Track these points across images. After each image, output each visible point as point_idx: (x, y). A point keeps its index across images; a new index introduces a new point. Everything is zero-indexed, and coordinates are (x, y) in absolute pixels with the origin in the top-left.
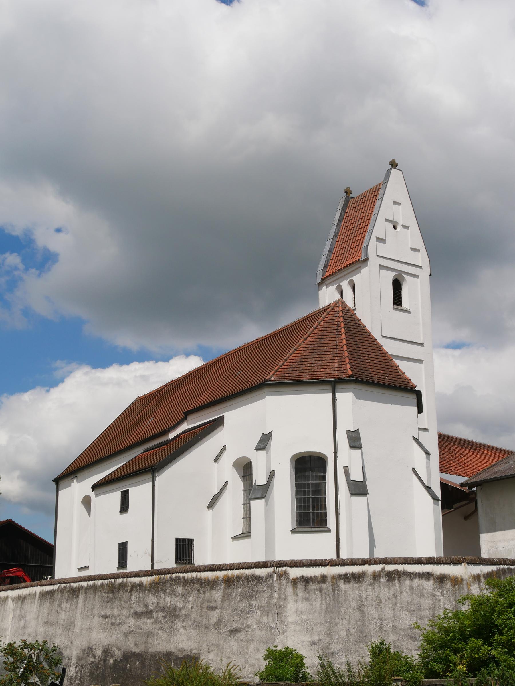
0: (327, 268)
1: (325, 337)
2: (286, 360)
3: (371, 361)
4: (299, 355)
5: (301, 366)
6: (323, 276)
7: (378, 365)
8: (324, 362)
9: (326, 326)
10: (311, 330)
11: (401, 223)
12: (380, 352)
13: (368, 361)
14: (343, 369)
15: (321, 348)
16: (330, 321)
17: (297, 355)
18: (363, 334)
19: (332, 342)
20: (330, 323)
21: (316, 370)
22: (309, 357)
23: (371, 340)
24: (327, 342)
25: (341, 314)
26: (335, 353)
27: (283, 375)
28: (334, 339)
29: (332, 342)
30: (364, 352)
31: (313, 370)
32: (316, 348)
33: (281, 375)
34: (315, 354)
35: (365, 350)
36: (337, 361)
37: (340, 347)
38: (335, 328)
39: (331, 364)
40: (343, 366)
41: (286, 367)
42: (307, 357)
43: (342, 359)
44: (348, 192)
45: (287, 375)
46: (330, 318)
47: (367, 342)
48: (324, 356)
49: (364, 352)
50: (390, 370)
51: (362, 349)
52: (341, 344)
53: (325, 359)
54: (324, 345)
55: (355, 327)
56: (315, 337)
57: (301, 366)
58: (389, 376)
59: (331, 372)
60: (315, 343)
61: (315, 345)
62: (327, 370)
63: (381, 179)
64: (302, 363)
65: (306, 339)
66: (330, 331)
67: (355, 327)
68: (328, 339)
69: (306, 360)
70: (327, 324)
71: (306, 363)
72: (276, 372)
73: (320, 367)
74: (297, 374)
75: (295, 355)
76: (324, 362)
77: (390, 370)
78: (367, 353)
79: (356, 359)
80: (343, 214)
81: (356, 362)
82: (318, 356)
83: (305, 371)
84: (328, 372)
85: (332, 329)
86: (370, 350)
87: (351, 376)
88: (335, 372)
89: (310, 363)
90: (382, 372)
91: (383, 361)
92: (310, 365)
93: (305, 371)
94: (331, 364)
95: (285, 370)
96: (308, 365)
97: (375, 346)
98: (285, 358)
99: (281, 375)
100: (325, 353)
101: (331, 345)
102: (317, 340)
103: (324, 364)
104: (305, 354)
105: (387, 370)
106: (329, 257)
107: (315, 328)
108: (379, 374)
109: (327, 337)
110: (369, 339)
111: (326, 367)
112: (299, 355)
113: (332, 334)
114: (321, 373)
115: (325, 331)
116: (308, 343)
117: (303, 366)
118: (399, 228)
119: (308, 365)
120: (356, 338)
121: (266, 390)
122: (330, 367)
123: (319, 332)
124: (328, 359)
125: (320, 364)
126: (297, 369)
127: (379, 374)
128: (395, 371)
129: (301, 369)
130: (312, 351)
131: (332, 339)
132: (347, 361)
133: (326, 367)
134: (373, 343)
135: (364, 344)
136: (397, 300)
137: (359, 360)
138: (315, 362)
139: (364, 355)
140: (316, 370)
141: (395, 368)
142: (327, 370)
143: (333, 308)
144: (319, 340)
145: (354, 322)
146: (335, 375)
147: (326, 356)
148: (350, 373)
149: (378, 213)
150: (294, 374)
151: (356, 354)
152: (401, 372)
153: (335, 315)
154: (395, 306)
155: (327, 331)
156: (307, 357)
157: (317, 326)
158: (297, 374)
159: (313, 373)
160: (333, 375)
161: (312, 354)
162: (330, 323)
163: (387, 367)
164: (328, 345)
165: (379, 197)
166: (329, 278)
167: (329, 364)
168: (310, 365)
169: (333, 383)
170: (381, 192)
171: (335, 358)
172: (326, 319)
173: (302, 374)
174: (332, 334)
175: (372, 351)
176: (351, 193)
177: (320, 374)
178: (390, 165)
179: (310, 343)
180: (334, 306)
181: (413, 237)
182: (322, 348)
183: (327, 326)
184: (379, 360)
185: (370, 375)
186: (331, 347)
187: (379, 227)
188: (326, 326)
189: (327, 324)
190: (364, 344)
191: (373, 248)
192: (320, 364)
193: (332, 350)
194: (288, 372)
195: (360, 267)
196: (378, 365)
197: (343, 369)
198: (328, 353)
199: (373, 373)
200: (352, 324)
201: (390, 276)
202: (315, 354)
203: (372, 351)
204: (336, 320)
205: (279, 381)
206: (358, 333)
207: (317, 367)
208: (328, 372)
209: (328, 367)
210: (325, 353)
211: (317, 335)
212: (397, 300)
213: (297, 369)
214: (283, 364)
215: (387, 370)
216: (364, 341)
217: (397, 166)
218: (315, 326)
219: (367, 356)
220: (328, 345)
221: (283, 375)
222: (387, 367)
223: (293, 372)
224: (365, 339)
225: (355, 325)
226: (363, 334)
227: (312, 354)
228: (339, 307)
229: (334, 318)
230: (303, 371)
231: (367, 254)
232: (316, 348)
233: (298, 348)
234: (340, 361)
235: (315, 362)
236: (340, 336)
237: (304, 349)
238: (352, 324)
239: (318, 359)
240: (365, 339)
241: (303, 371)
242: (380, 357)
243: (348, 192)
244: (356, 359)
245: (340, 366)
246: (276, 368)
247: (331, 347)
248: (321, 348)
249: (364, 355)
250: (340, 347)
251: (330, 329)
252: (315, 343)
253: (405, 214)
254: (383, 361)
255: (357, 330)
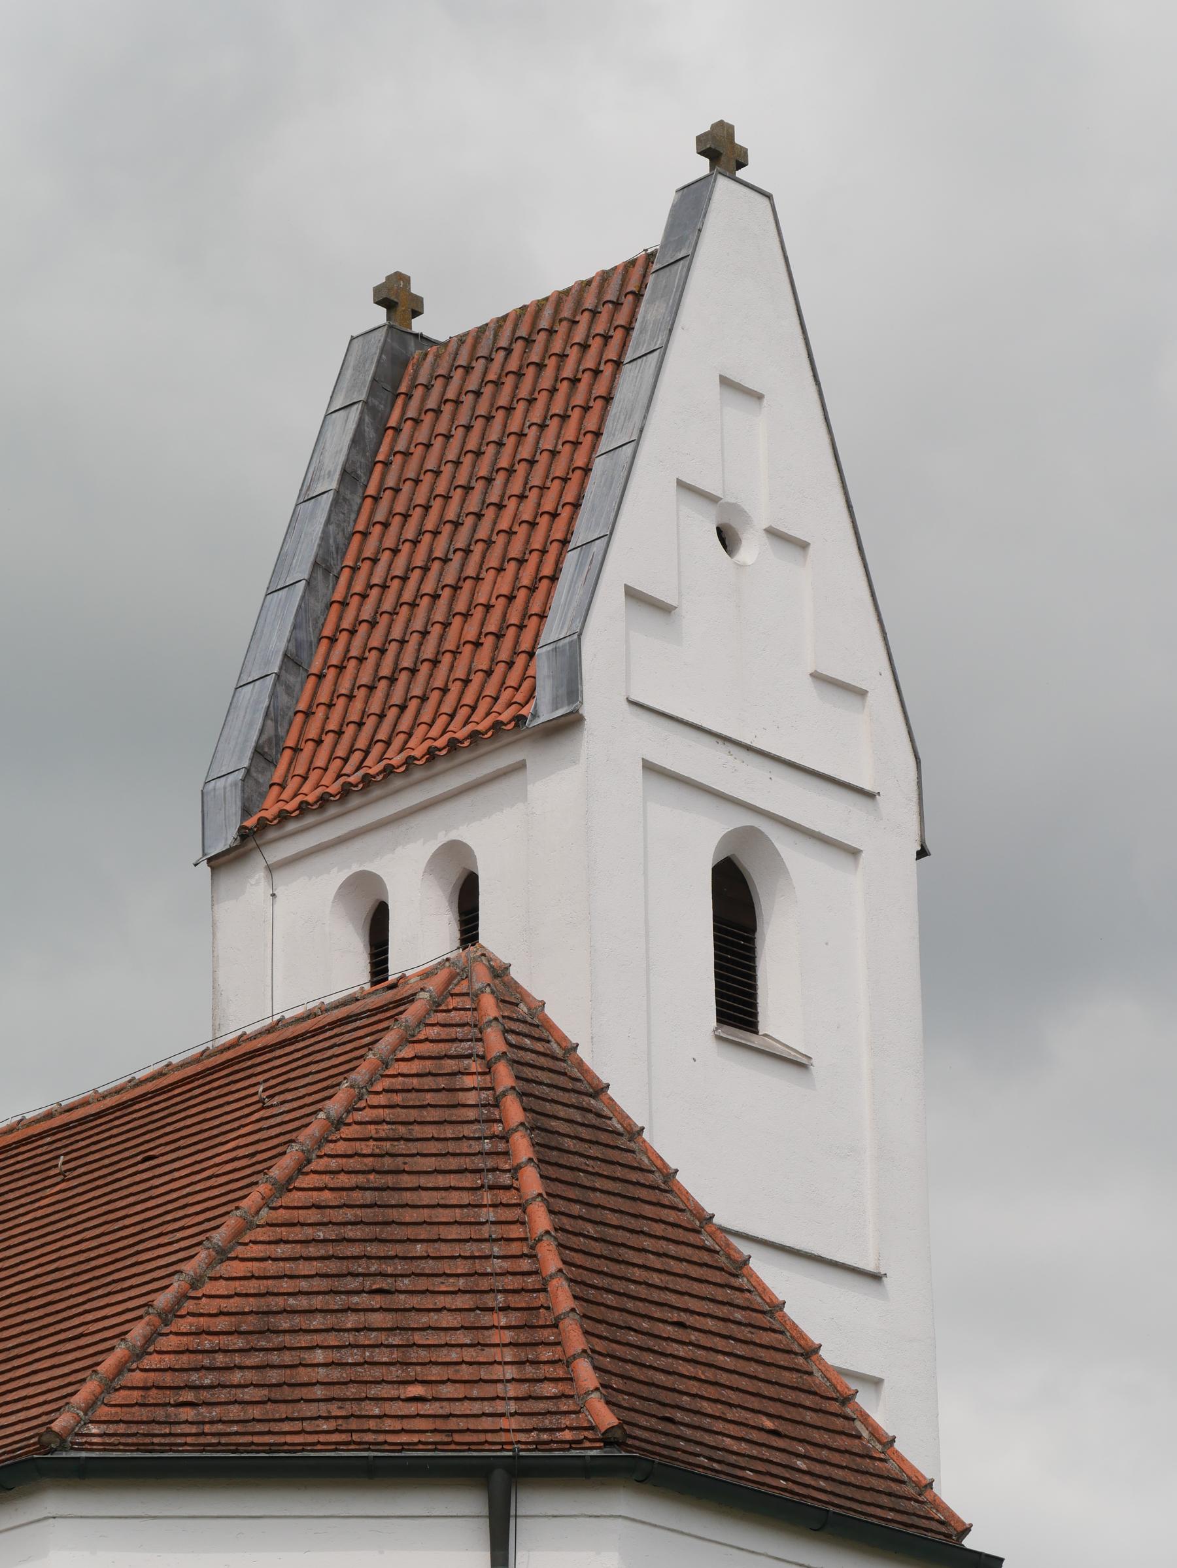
0: (273, 763)
1: (407, 1181)
2: (170, 1314)
3: (700, 1354)
4: (252, 1286)
5: (275, 1358)
6: (246, 812)
7: (744, 1383)
8: (418, 1338)
9: (403, 1115)
10: (315, 1128)
11: (761, 512)
12: (738, 1298)
13: (681, 1351)
14: (551, 1389)
15: (391, 1250)
16: (429, 1082)
17: (240, 1286)
18: (634, 1176)
19: (458, 1214)
20: (430, 1098)
21: (373, 1391)
22: (318, 1302)
23: (683, 1219)
24: (425, 1214)
25: (495, 1042)
26: (484, 1284)
27: (160, 1414)
28: (466, 1198)
29: (458, 1214)
30: (656, 1295)
31: (352, 1391)
32: (354, 1250)
33: (143, 1414)
34: (354, 1284)
35: (656, 1279)
36: (507, 1336)
37: (515, 1248)
38: (467, 1130)
39: (469, 1354)
40: (549, 1371)
41: (168, 1361)
42: (304, 1302)
43: (535, 1326)
44: (397, 298)
45: (188, 1413)
46: (429, 1065)
47: (658, 1229)
48: (414, 1301)
49: (656, 1295)
50: (809, 1417)
51: (638, 1274)
52: (516, 1231)
53: (424, 1319)
54: (411, 1232)
55: (584, 1133)
56: (343, 1180)
57: (275, 1358)
58: (813, 1452)
59: (476, 1407)
60: (349, 1214)
61: (350, 1232)
62: (447, 1391)
63: (647, 234)
64: (277, 1340)
65: (286, 1186)
66: (433, 1147)
67: (584, 1133)
68: (427, 1198)
69: (298, 1321)
70: (413, 1099)
71: (304, 1340)
72: (109, 1386)
73: (395, 1373)
74: (256, 1412)
75: (221, 1287)
76: (418, 1338)
77: (809, 1417)
78: (673, 1299)
79: (620, 1335)
80: (370, 433)
81: (619, 1350)
82: (376, 1301)
83: (305, 1393)
84: (458, 1408)
85: (449, 1132)
86: (683, 1285)
87: (608, 1440)
88: (500, 1407)
89: (332, 1339)
90: (769, 1424)
91: (763, 1354)
92: (335, 1356)
93: (305, 1393)
94: (469, 1354)
95: (168, 1379)
96: (319, 1356)
97: (706, 1257)
98: (162, 1300)
99: (143, 1414)
100: (422, 1284)
101: (454, 1232)
102: (357, 1197)
103: (423, 1355)
104: (286, 1285)
105: (794, 1413)
106: (284, 699)
107: (339, 1123)
108: (754, 1435)
109: (423, 1181)
110: (672, 1216)
111: (435, 1373)
112: (252, 1286)
113: (453, 1163)
114: (412, 1408)
115: (401, 1147)
116: (303, 1216)
117: (287, 1358)
118: (752, 548)
119: (319, 1356)
120: (597, 1198)
121: (51, 1503)
122: (465, 1372)
123: (367, 1148)
124: (447, 1320)
125: (396, 1355)
126: (249, 1376)
127: (754, 1435)
128: (839, 1423)
129: (274, 1376)
130: (332, 1267)
131: (454, 1198)
132: (575, 1340)
133: (435, 1373)
134: (691, 1238)
135: (647, 1243)
136: (737, 1003)
137: (632, 1338)
138: (362, 1339)
139: (656, 1312)
140: (373, 1391)
141: (834, 1407)
142: (447, 1391)
143: (436, 1006)
144: (369, 1197)
145: (573, 1099)
146: (509, 1428)
147: (427, 1302)
148: (607, 1418)
149: (637, 442)
150: (235, 1412)
151: (610, 1299)
152: (875, 1431)
153: (454, 1049)
154: (720, 1032)
155: (414, 1148)
156: (304, 1302)
157: (351, 1109)
158: (256, 1412)
159: (355, 1408)
160: (487, 1423)
161: (339, 1284)
162: (430, 1098)
163: (791, 1396)
164: (433, 1232)
165: (639, 343)
166: (292, 826)
167: (454, 1355)
168: (335, 1356)
169: (499, 1476)
170: (649, 312)
171: (486, 1319)
172: (403, 1067)
173: (283, 1410)
174: (453, 1163)
175: (696, 1288)
176: (416, 313)
177: (402, 1417)
178: (702, 153)
179: (313, 1216)
180: (447, 992)
181: (811, 609)
182: (399, 1249)
183: (413, 1114)
184: (740, 1349)
185: (708, 1439)
186: (457, 1250)
187: (644, 531)
188: (403, 1115)
189: (413, 1099)
190: (647, 1243)
191: (612, 656)
192: (396, 1355)
193: (461, 1267)
194: (189, 1396)
195: (521, 766)
196: (744, 1383)
197: (551, 1389)
198: (437, 1284)
199: (719, 1426)
200: (562, 1112)
201: (700, 840)
202: (354, 1284)
203: (696, 1288)
204: (469, 1082)
205: (138, 1447)
206: (606, 1170)
207: (377, 1373)
208: (458, 1408)
209: (450, 1372)
210: (422, 1284)
211: (352, 1163)
212: (737, 1003)
213: (249, 1376)
214: (149, 1340)
215: (794, 1413)
216: (646, 1226)
217: (741, 165)
218: (334, 1107)
219: (675, 1316)
220: (433, 1232)
221: (160, 1414)
222: (791, 1396)
223: (223, 1395)
224: (648, 1210)
225: (577, 1116)
226: (634, 1176)
227: (339, 1284)
228: (475, 996)
229: (450, 1065)
230: (287, 1393)
231: (572, 688)
232: (354, 1250)
233: (236, 1239)
234: (523, 1337)
235: (362, 1339)
236: (506, 1179)
237: (280, 1250)
238: (562, 1112)
239: (376, 1319)
240: (648, 1210)
241: (287, 1393)
242: (746, 1333)
243: (397, 298)
244: (620, 1335)
245: (530, 1371)
246: (109, 1364)
247: (457, 1250)
248: (391, 1250)
249: (656, 1312)
250: (515, 1248)
251: (430, 1131)
252: (349, 1214)
253: (772, 465)
254: (763, 1354)
255: (594, 1151)
